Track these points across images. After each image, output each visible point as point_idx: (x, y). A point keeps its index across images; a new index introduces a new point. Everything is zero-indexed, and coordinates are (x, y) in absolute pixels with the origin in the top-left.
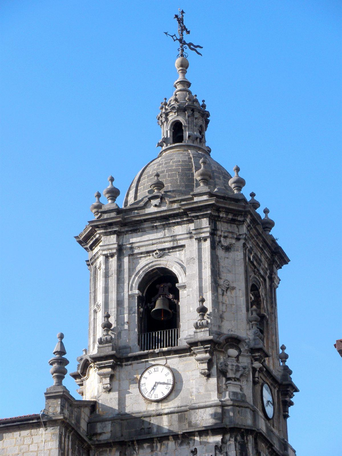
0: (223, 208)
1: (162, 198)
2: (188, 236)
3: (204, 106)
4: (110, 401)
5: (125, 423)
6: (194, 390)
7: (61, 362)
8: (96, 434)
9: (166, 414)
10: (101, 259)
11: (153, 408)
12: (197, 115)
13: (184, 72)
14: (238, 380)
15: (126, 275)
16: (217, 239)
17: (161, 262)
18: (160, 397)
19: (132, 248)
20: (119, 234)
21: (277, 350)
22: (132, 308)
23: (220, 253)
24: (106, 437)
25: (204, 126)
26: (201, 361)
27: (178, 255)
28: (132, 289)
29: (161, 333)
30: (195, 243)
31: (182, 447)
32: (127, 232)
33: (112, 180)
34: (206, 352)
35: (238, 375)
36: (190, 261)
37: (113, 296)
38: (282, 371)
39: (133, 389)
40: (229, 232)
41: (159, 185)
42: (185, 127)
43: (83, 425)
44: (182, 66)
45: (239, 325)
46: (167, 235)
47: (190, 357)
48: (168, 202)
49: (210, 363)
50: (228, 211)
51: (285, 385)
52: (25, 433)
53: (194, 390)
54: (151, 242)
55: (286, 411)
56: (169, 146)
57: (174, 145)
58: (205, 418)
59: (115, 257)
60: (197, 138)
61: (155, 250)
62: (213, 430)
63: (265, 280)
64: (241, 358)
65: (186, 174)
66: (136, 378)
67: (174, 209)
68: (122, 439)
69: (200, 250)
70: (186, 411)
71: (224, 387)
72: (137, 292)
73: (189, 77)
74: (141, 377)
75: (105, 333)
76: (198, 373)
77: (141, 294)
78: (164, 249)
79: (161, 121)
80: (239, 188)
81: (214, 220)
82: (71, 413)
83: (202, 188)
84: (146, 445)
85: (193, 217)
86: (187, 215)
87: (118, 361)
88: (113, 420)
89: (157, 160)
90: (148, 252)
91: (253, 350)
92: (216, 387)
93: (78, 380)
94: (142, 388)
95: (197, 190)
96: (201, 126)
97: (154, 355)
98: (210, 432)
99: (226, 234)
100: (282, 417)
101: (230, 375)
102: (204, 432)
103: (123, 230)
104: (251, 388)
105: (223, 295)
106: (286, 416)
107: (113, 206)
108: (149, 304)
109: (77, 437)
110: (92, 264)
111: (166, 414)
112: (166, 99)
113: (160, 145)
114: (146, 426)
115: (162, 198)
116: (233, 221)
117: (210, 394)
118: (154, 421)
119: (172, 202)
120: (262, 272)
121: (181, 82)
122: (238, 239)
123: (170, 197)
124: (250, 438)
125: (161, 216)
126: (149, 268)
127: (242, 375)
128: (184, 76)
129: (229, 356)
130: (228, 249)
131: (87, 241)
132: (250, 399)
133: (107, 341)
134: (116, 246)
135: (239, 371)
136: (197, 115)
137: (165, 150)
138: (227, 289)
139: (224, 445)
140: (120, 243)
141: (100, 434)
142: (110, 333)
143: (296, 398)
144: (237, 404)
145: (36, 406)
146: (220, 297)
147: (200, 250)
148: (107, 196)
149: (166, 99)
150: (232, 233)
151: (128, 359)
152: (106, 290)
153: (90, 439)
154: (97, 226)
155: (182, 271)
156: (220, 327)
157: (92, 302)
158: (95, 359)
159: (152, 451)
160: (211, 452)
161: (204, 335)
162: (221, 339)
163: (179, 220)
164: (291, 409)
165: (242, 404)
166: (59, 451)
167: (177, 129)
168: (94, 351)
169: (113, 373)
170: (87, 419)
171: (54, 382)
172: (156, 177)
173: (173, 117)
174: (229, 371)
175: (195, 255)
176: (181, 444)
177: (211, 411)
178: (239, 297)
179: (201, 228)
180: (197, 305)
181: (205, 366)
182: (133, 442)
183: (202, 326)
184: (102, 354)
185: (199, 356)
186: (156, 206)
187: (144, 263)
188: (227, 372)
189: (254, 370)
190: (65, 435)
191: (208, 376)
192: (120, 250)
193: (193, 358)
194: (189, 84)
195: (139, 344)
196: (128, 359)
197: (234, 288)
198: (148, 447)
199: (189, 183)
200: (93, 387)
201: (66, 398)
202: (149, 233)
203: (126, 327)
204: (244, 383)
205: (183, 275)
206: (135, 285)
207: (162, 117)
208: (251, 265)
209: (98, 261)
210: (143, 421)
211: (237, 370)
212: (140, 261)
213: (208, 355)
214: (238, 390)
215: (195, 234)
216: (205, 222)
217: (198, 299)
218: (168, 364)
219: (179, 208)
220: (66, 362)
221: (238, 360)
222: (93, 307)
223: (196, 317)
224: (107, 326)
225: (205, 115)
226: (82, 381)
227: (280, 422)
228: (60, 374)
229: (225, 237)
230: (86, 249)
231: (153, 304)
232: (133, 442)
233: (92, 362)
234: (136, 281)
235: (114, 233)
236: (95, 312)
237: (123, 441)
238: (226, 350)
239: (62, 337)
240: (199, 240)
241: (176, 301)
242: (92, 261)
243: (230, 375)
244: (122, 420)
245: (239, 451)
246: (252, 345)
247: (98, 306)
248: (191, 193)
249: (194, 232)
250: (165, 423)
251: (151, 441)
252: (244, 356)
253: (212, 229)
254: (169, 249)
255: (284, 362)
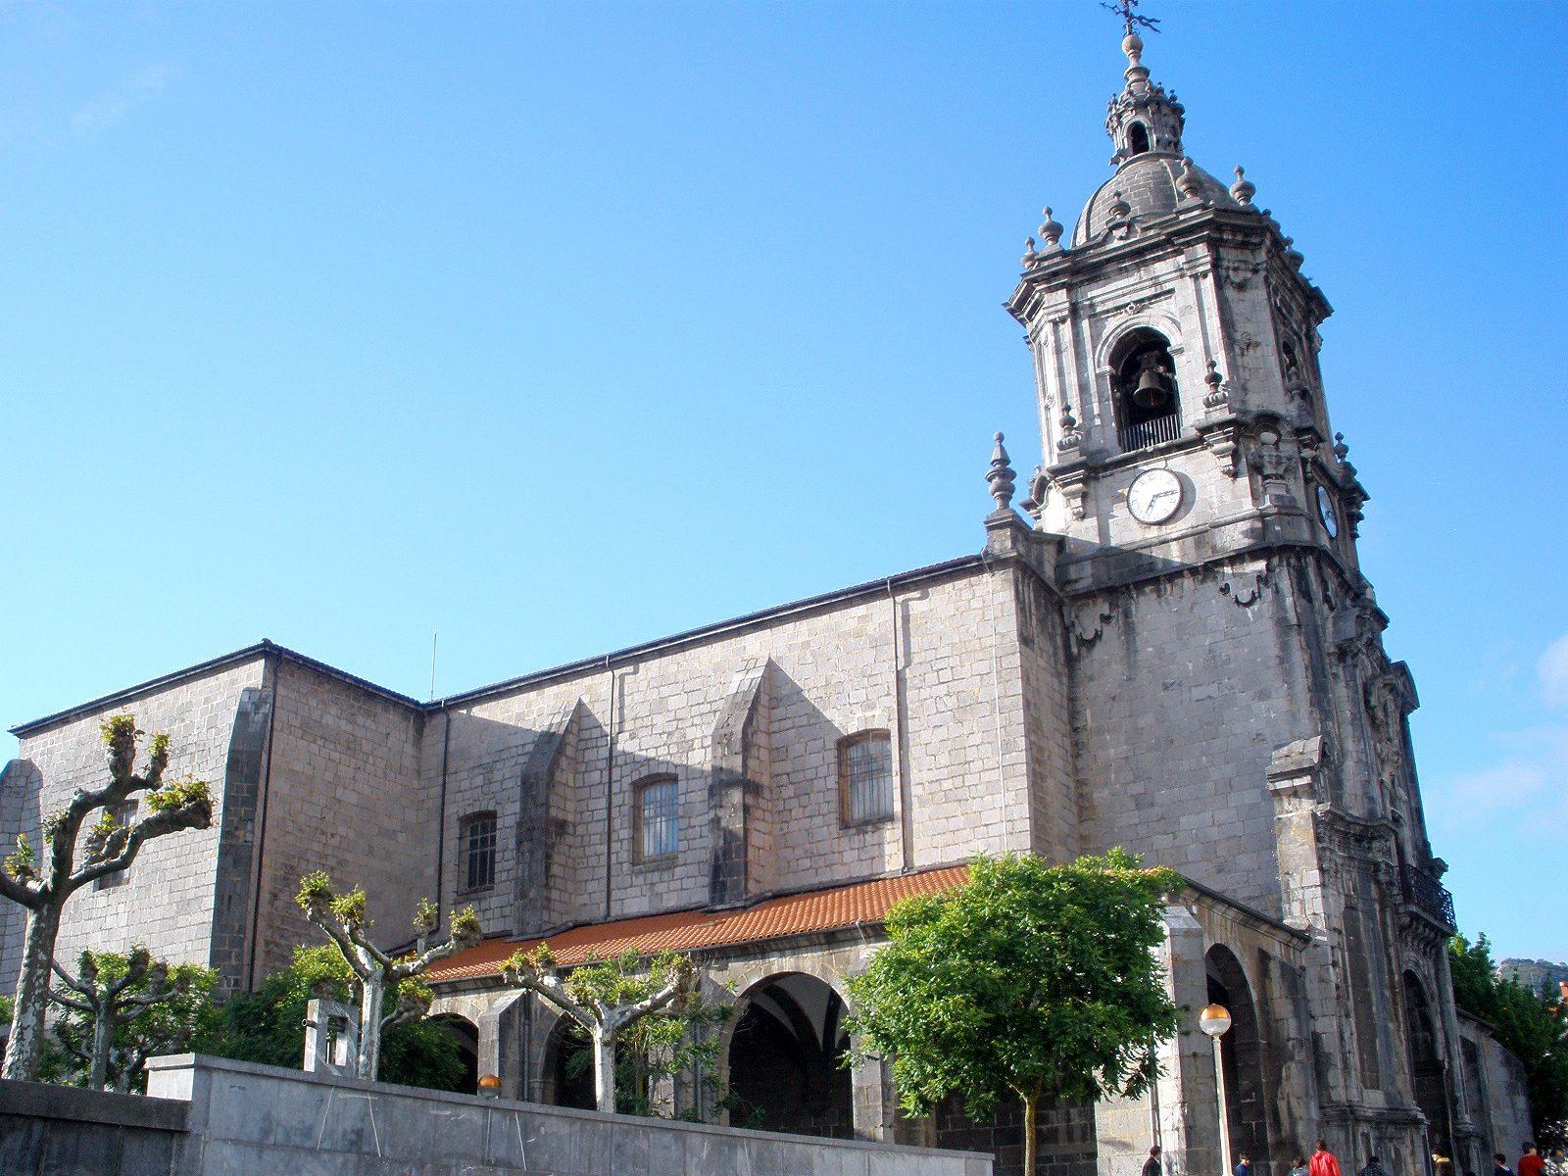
0: (1226, 224)
1: (1130, 226)
2: (1178, 274)
3: (1174, 98)
4: (1085, 532)
5: (1112, 560)
6: (1215, 500)
7: (1004, 474)
8: (1069, 582)
9: (1175, 540)
10: (1048, 328)
11: (1153, 533)
12: (1165, 110)
13: (1137, 56)
14: (1282, 477)
15: (1088, 346)
16: (1223, 273)
17: (1141, 320)
18: (1163, 516)
19: (1092, 306)
20: (1070, 288)
21: (1331, 443)
22: (1104, 392)
23: (1230, 293)
24: (1085, 584)
25: (1177, 125)
26: (1221, 453)
27: (1165, 305)
28: (1100, 364)
29: (1148, 424)
30: (1189, 282)
31: (1205, 585)
32: (1082, 283)
33: (1049, 212)
34: (1227, 440)
35: (1281, 471)
36: (1185, 311)
37: (1072, 379)
38: (1342, 470)
39: (1119, 510)
40: (1240, 261)
41: (1123, 208)
42: (1150, 129)
43: (1049, 572)
44: (1132, 47)
45: (1271, 396)
46: (1145, 278)
47: (1202, 452)
48: (1139, 230)
49: (1235, 455)
50: (1235, 229)
51: (1349, 489)
52: (961, 584)
53: (1215, 500)
54: (1120, 292)
55: (1353, 528)
56: (1129, 159)
57: (1136, 156)
58: (1235, 538)
59: (1069, 321)
60: (1170, 143)
61: (1129, 304)
62: (1252, 554)
63: (1300, 339)
64: (1282, 446)
65: (1162, 190)
66: (1122, 494)
67: (1151, 237)
68: (1110, 584)
69: (1198, 292)
70: (1207, 531)
71: (1261, 489)
72: (1108, 368)
73: (1144, 63)
74: (1129, 492)
75: (1067, 433)
76: (1217, 474)
77: (1114, 372)
78: (1142, 301)
79: (1112, 127)
80: (1247, 198)
81: (1214, 245)
82: (1028, 550)
83: (1190, 200)
84: (1147, 589)
85: (1183, 244)
86: (1173, 245)
87: (1093, 472)
88: (1093, 558)
89: (1115, 179)
90: (1118, 308)
91: (1299, 432)
92: (1249, 490)
93: (1032, 511)
94: (1134, 507)
95: (1180, 206)
96: (1173, 127)
97: (1146, 456)
98: (1246, 556)
99: (1236, 265)
100: (1348, 538)
101: (1268, 471)
102: (1237, 558)
103: (1075, 281)
104: (1303, 488)
105: (1243, 355)
106: (1354, 536)
107: (1056, 248)
108: (1128, 386)
109: (1041, 585)
110: (1034, 340)
111: (1175, 540)
112: (1115, 95)
113: (1115, 161)
114: (1145, 562)
115: (1130, 226)
116: (1243, 245)
117: (1241, 502)
118: (1157, 553)
119: (1145, 229)
120: (1295, 327)
121: (1135, 70)
122: (1255, 271)
123: (1142, 222)
124: (1310, 560)
125: (1132, 251)
126: (1123, 330)
127: (1286, 470)
128: (1137, 61)
129: (1263, 444)
130: (1241, 287)
131: (1022, 307)
132: (1301, 502)
133: (1071, 445)
134: (1067, 305)
135: (1281, 463)
136: (1165, 110)
137: (1124, 167)
138: (1249, 345)
139: (1270, 574)
140: (1074, 301)
141: (1076, 581)
142: (1073, 432)
143: (1366, 509)
144: (1284, 511)
145: (974, 543)
146: (1239, 358)
147: (1198, 292)
148: (1045, 235)
149: (1115, 95)
150: (1245, 262)
151: (1106, 467)
152: (1061, 373)
153: (1061, 590)
154: (1035, 280)
155: (1174, 328)
156: (1243, 402)
157: (1041, 395)
158: (1056, 472)
159: (1159, 596)
160: (1252, 586)
161: (1221, 414)
162: (1249, 419)
163: (1161, 253)
164: (1360, 525)
165: (1294, 511)
166: (1017, 604)
167: (1138, 135)
168: (1052, 461)
169: (1085, 490)
170: (1053, 562)
171: (998, 504)
172: (1116, 198)
173: (1129, 118)
174: (1267, 464)
175: (1192, 300)
176: (1203, 581)
177: (1245, 526)
178: (1267, 356)
179: (1197, 259)
180: (1205, 373)
181: (1228, 461)
182: (1127, 587)
183: (1217, 402)
184: (1066, 464)
185: (1217, 447)
186: (1121, 238)
187: (1114, 326)
188: (1263, 466)
189: (1304, 461)
190: (1023, 582)
191: (1235, 475)
192: (1075, 311)
193: (1208, 452)
194: (1146, 72)
195: (1120, 445)
196: (1106, 467)
197: (1257, 344)
198: (1152, 591)
199: (1166, 197)
200: (1058, 516)
201: (1018, 527)
202: (1116, 280)
203: (1098, 422)
204: (1291, 483)
205: (1177, 334)
206: (1104, 358)
207: (1112, 121)
208: (1279, 315)
209: (1042, 335)
210: (1140, 554)
211: (1279, 463)
212: (1106, 323)
213: (1231, 443)
214: (1283, 493)
215: (1188, 269)
216: (1201, 250)
217: (1206, 364)
218: (1169, 467)
219: (1159, 235)
220: (1013, 475)
221: (1277, 449)
222: (1042, 403)
223: (1206, 390)
224: (1068, 423)
225: (1178, 111)
226: (1039, 512)
227: (1346, 544)
228: (1006, 492)
229: (1236, 269)
230: (1021, 321)
231: (1134, 384)
232: (1127, 587)
233: (1052, 479)
234: (1105, 353)
235: (1062, 286)
236: (1047, 408)
237: (1112, 587)
238: (1258, 435)
239: (1001, 438)
240: (1195, 277)
241: (1170, 375)
242: (1034, 335)
243: (1268, 471)
244: (1107, 556)
245: (1295, 580)
246: (1297, 424)
247: (1051, 398)
248: (1174, 210)
249: (1186, 266)
250: (1175, 554)
251: (1155, 581)
252: (1285, 441)
253: (1214, 259)
254: (1150, 298)
255: (1342, 457)
